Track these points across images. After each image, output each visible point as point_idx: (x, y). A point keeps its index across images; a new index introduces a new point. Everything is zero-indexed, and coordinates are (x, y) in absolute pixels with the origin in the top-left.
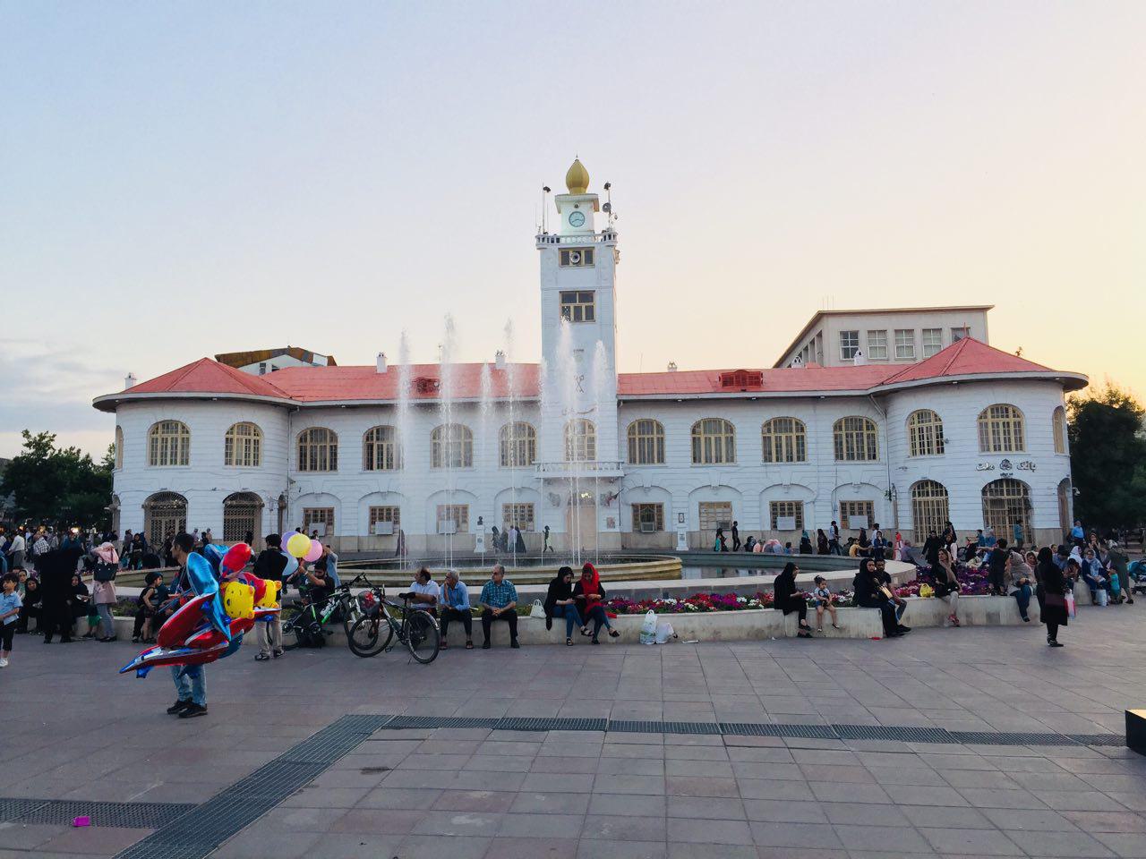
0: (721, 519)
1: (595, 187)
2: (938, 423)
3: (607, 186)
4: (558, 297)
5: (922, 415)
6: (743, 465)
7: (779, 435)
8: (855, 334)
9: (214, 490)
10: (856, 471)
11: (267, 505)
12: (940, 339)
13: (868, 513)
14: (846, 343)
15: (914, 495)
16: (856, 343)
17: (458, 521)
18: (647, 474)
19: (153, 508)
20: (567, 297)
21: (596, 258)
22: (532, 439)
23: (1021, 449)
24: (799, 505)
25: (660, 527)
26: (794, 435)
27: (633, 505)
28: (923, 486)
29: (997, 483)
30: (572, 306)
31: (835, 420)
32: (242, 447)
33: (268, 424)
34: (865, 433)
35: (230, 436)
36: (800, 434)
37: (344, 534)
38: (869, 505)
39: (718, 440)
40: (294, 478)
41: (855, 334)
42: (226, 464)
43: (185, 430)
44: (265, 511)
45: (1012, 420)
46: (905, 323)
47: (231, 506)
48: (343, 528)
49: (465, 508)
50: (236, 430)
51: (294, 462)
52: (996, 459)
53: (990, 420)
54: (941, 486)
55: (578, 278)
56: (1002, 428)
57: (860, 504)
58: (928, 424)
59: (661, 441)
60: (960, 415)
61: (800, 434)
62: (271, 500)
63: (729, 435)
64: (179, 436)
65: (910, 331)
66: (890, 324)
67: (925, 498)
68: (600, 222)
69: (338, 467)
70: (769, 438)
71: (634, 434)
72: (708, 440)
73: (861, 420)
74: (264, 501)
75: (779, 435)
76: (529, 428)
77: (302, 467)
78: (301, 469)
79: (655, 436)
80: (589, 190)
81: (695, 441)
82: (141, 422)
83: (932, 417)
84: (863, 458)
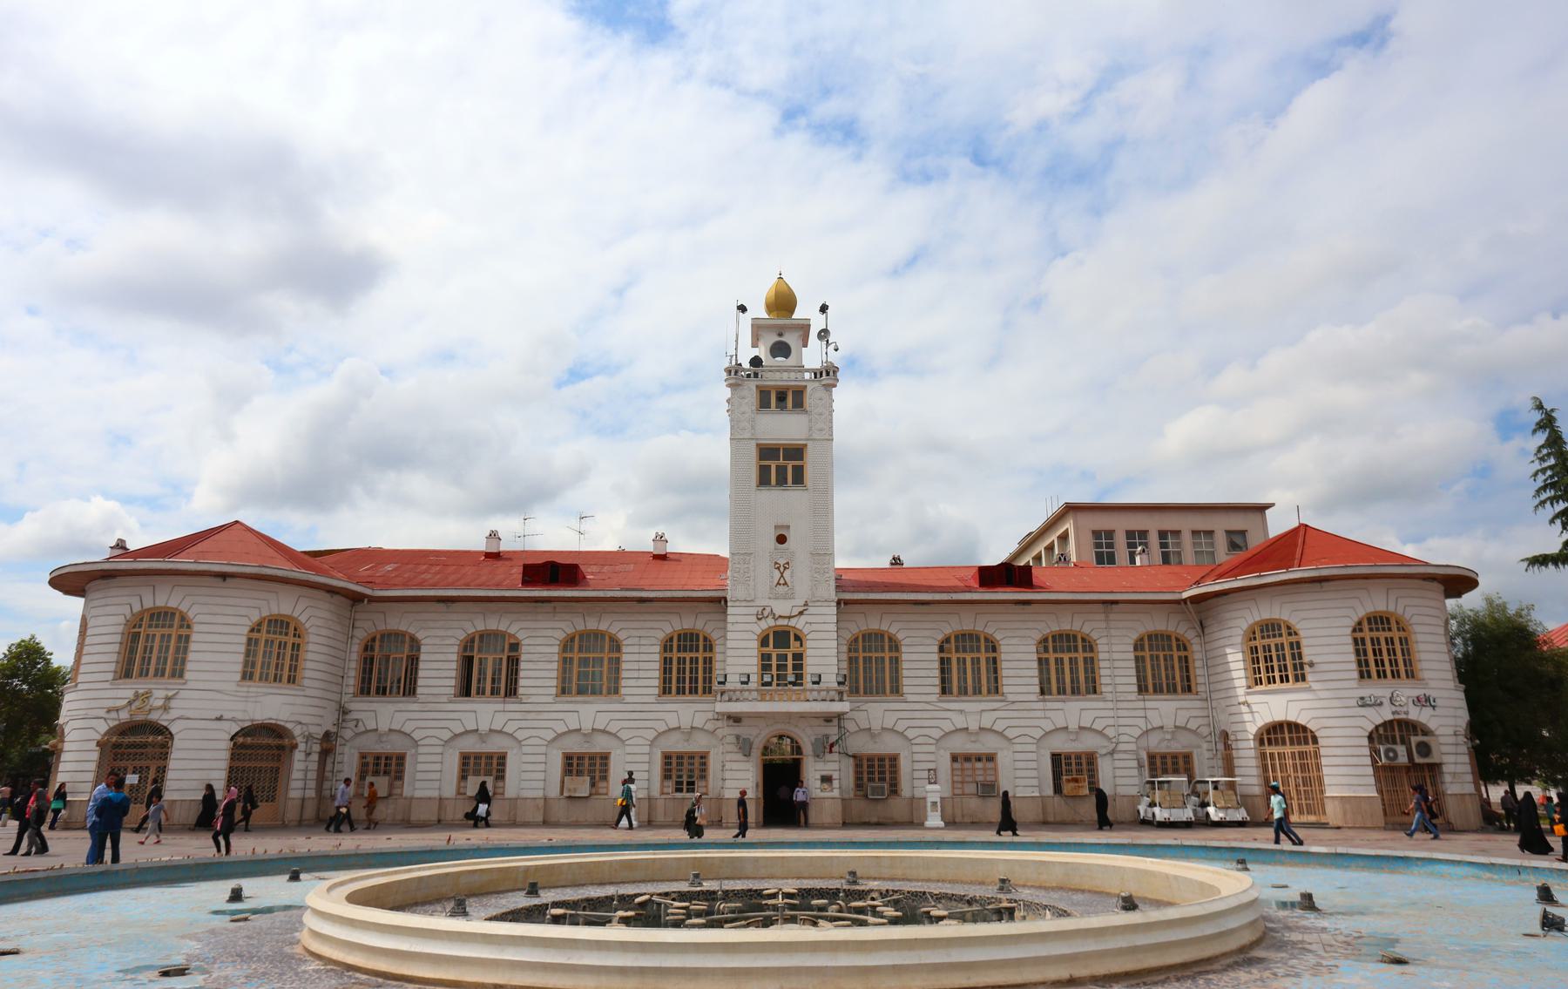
0: (980, 778)
1: (805, 310)
2: (1293, 639)
3: (824, 309)
4: (753, 453)
5: (1270, 628)
6: (1011, 698)
7: (1059, 655)
8: (1110, 534)
9: (220, 719)
10: (1167, 710)
11: (302, 747)
12: (1212, 545)
13: (590, 771)
14: (1098, 545)
15: (1262, 742)
16: (1110, 546)
17: (593, 778)
18: (877, 713)
19: (116, 746)
20: (767, 452)
21: (809, 400)
22: (708, 655)
23: (1411, 675)
24: (1091, 759)
25: (894, 790)
26: (983, 656)
27: (854, 757)
28: (1275, 732)
29: (1387, 725)
30: (773, 465)
31: (1135, 636)
32: (273, 650)
33: (316, 620)
34: (1176, 654)
35: (255, 635)
36: (1089, 655)
37: (418, 794)
38: (1188, 757)
39: (976, 662)
40: (352, 706)
41: (1110, 534)
42: (244, 678)
43: (1291, 631)
44: (298, 755)
45: (1396, 635)
46: (1170, 522)
47: (243, 746)
48: (418, 784)
49: (605, 757)
50: (265, 628)
51: (352, 682)
52: (126, 691)
53: (1367, 635)
54: (1305, 729)
55: (783, 427)
56: (1381, 650)
57: (1175, 757)
58: (1278, 640)
59: (896, 661)
60: (1325, 631)
61: (1089, 655)
62: (309, 738)
63: (1183, 654)
64: (700, 655)
65: (1210, 533)
66: (1186, 524)
67: (1281, 749)
68: (812, 356)
69: (521, 691)
70: (1143, 658)
71: (856, 651)
72: (1059, 661)
73: (1169, 637)
74: (299, 739)
75: (1059, 655)
76: (705, 639)
77: (364, 690)
78: (362, 693)
79: (887, 655)
80: (798, 314)
81: (944, 665)
82: (117, 609)
83: (1284, 631)
84: (1175, 691)
